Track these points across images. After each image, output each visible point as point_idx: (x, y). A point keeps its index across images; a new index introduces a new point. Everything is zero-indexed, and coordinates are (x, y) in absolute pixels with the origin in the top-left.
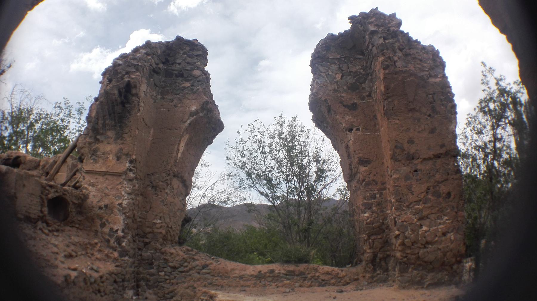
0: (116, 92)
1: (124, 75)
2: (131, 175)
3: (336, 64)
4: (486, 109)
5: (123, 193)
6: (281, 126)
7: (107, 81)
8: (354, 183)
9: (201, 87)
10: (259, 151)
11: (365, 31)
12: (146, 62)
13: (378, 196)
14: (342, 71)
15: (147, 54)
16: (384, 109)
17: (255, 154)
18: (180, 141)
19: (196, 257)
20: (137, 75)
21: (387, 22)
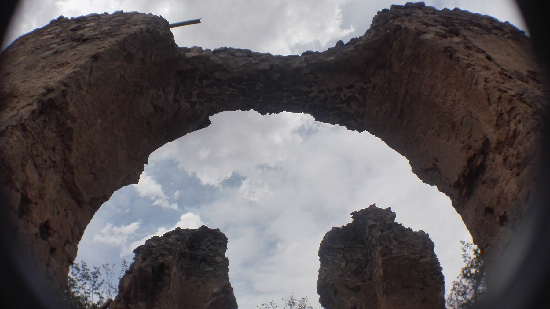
0: (150, 270)
1: (158, 257)
3: (340, 253)
4: (469, 275)
7: (141, 259)
9: (222, 272)
12: (176, 247)
14: (346, 259)
15: (178, 240)
16: (383, 290)
20: (171, 258)
21: (384, 216)
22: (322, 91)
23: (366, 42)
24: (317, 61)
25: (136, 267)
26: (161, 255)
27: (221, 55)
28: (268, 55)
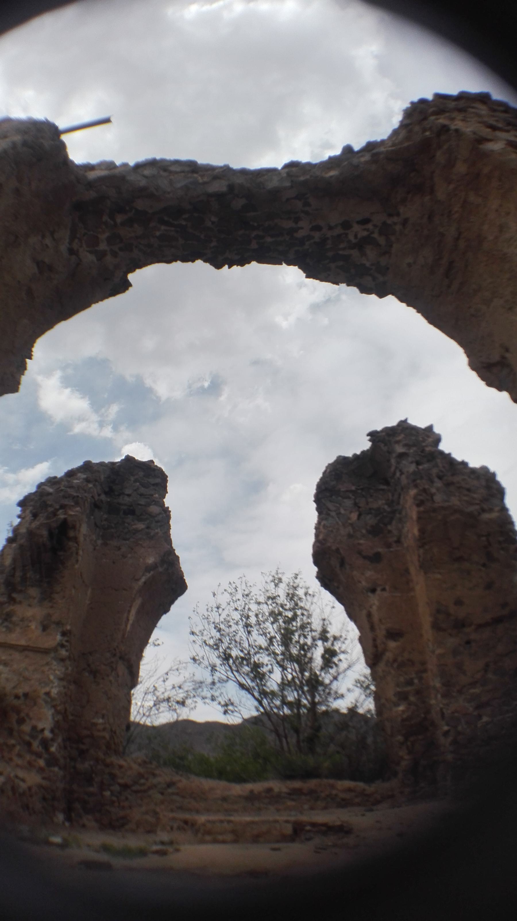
1: (58, 510)
2: (64, 653)
3: (349, 498)
5: (52, 677)
6: (276, 585)
7: (31, 515)
8: (381, 667)
10: (241, 622)
11: (389, 452)
13: (416, 681)
14: (359, 507)
15: (88, 480)
17: (234, 628)
18: (131, 607)
19: (157, 772)
20: (77, 511)
21: (421, 439)
22: (317, 228)
23: (390, 148)
24: (308, 177)
25: (23, 530)
26: (63, 507)
27: (147, 172)
28: (225, 168)
